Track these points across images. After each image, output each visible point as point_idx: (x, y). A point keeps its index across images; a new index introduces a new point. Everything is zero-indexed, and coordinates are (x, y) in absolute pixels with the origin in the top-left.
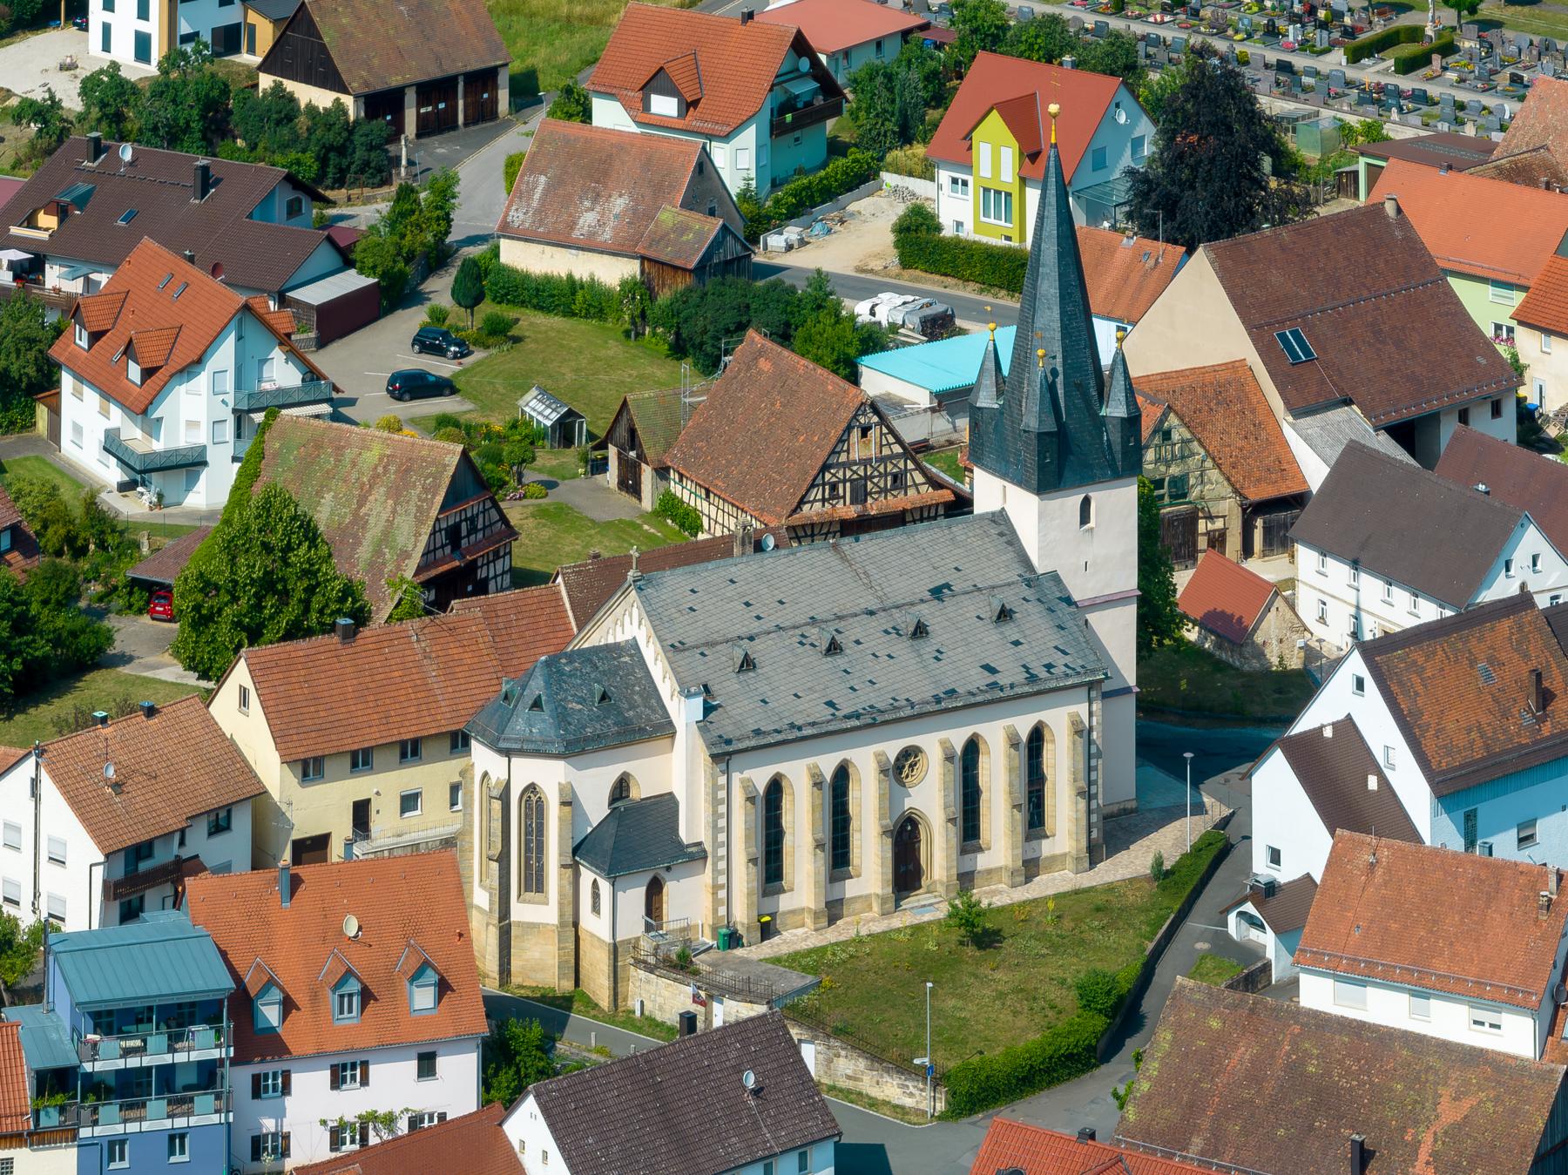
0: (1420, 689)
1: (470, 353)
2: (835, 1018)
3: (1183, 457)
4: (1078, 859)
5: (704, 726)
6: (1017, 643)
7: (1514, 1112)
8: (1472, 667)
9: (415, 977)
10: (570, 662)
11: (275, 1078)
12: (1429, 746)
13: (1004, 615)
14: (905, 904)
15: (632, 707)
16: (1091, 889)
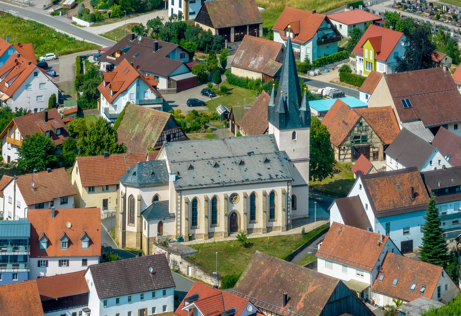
0: (377, 189)
1: (215, 96)
2: (198, 261)
3: (366, 131)
4: (283, 228)
5: (175, 182)
6: (269, 169)
7: (326, 290)
8: (394, 185)
9: (83, 239)
10: (146, 164)
11: (44, 262)
12: (376, 204)
13: (267, 161)
14: (232, 235)
15: (160, 177)
16: (284, 236)
